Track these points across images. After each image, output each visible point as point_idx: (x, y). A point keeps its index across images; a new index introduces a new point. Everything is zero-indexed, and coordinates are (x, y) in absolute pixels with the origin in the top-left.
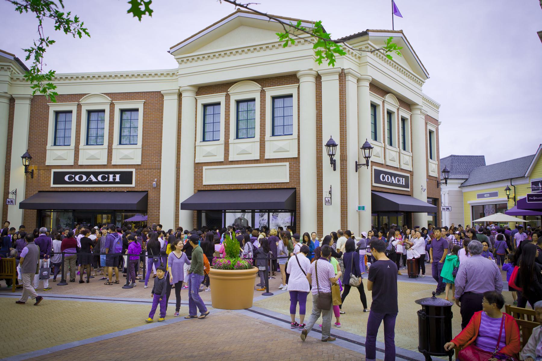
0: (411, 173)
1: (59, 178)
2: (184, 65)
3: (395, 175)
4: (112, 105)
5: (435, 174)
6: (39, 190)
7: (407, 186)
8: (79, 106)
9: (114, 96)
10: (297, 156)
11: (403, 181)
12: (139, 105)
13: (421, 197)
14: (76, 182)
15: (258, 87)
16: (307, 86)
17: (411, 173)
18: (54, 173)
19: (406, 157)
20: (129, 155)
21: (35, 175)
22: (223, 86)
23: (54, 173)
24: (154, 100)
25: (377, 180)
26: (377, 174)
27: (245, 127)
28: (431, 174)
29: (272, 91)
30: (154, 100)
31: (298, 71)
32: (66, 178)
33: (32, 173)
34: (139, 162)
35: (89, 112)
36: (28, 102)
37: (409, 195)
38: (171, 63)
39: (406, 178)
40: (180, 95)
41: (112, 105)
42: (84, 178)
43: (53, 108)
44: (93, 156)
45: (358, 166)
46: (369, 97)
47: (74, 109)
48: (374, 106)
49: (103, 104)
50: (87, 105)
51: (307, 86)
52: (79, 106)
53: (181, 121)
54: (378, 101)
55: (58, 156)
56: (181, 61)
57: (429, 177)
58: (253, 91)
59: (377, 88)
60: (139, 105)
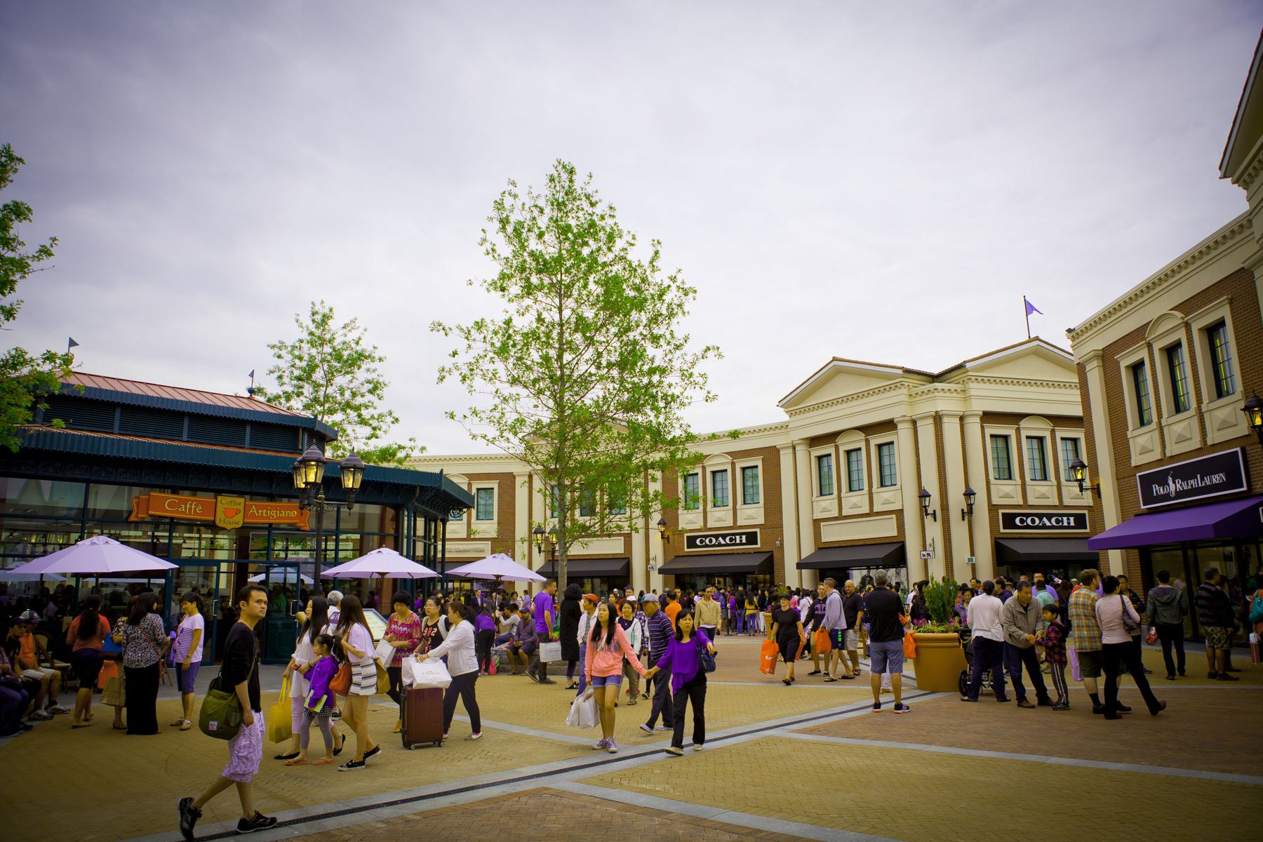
1: (691, 542)
4: (733, 464)
12: (494, 485)
15: (861, 436)
20: (753, 515)
24: (771, 456)
29: (876, 440)
30: (771, 456)
35: (714, 473)
38: (782, 416)
40: (794, 448)
41: (733, 464)
43: (1079, 434)
44: (720, 518)
49: (723, 463)
51: (903, 436)
53: (797, 473)
55: (689, 520)
58: (857, 441)
60: (494, 485)
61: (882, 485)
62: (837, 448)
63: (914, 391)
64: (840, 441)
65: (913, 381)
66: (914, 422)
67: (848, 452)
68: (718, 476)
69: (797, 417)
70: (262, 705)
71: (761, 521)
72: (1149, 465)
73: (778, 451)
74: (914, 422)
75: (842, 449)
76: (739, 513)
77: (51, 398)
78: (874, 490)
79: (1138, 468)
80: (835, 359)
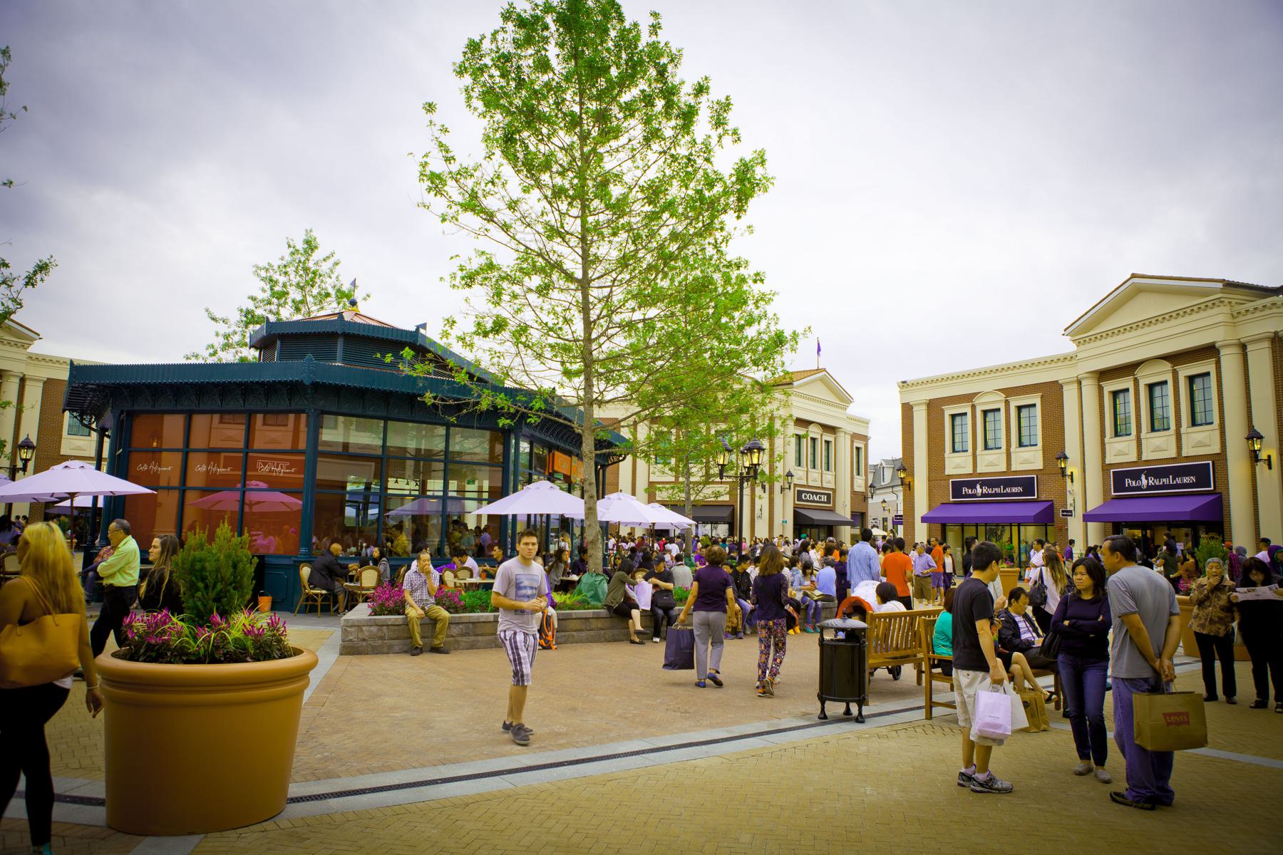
0: (834, 490)
2: (1082, 347)
3: (817, 494)
4: (1007, 403)
5: (862, 489)
7: (828, 502)
8: (973, 407)
9: (1010, 392)
11: (824, 498)
12: (1036, 399)
13: (844, 510)
15: (1167, 366)
16: (1230, 360)
17: (834, 490)
19: (829, 477)
20: (1029, 460)
22: (1129, 369)
24: (1052, 393)
25: (800, 499)
26: (800, 493)
28: (856, 489)
29: (1185, 371)
30: (1052, 393)
34: (1041, 467)
35: (985, 413)
37: (832, 510)
38: (1068, 346)
39: (829, 495)
40: (1080, 383)
41: (1007, 403)
43: (949, 411)
45: (782, 489)
46: (792, 429)
47: (969, 411)
48: (799, 437)
49: (997, 401)
50: (982, 404)
51: (1230, 360)
52: (973, 407)
53: (1082, 414)
54: (801, 432)
55: (957, 465)
56: (1079, 343)
57: (854, 493)
58: (1163, 372)
59: (801, 422)
60: (1036, 399)
61: (1194, 424)
62: (1136, 381)
63: (1242, 308)
64: (1139, 373)
65: (1236, 297)
66: (1243, 347)
67: (1151, 387)
68: (958, 420)
69: (1087, 346)
70: (348, 658)
71: (1039, 465)
72: (960, 476)
73: (1061, 387)
74: (1243, 347)
75: (1142, 383)
76: (1107, 446)
77: (102, 388)
78: (1183, 430)
79: (950, 476)
80: (1134, 276)
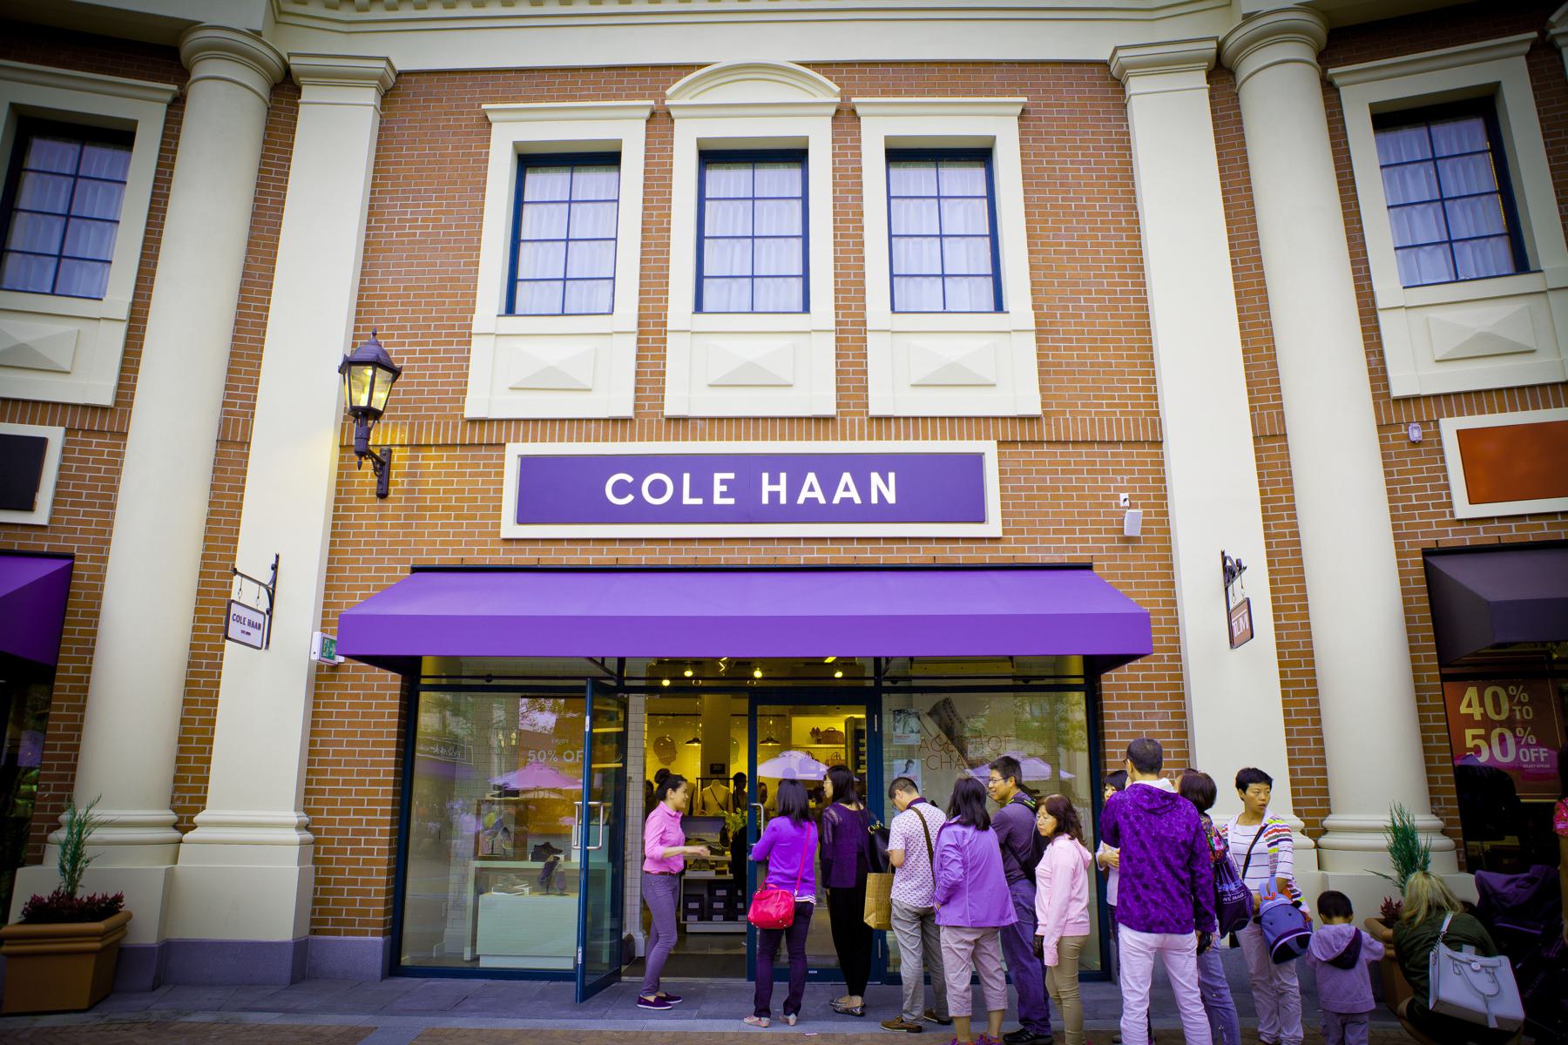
1: (555, 489)
6: (1429, 542)
10: (107, 399)
12: (991, 119)
14: (775, 514)
18: (527, 462)
20: (965, 363)
21: (398, 481)
23: (527, 462)
27: (1461, 229)
31: (192, 25)
32: (884, 488)
33: (382, 466)
36: (370, 96)
41: (845, 119)
42: (811, 489)
44: (751, 365)
47: (630, 135)
52: (660, 121)
55: (541, 366)
